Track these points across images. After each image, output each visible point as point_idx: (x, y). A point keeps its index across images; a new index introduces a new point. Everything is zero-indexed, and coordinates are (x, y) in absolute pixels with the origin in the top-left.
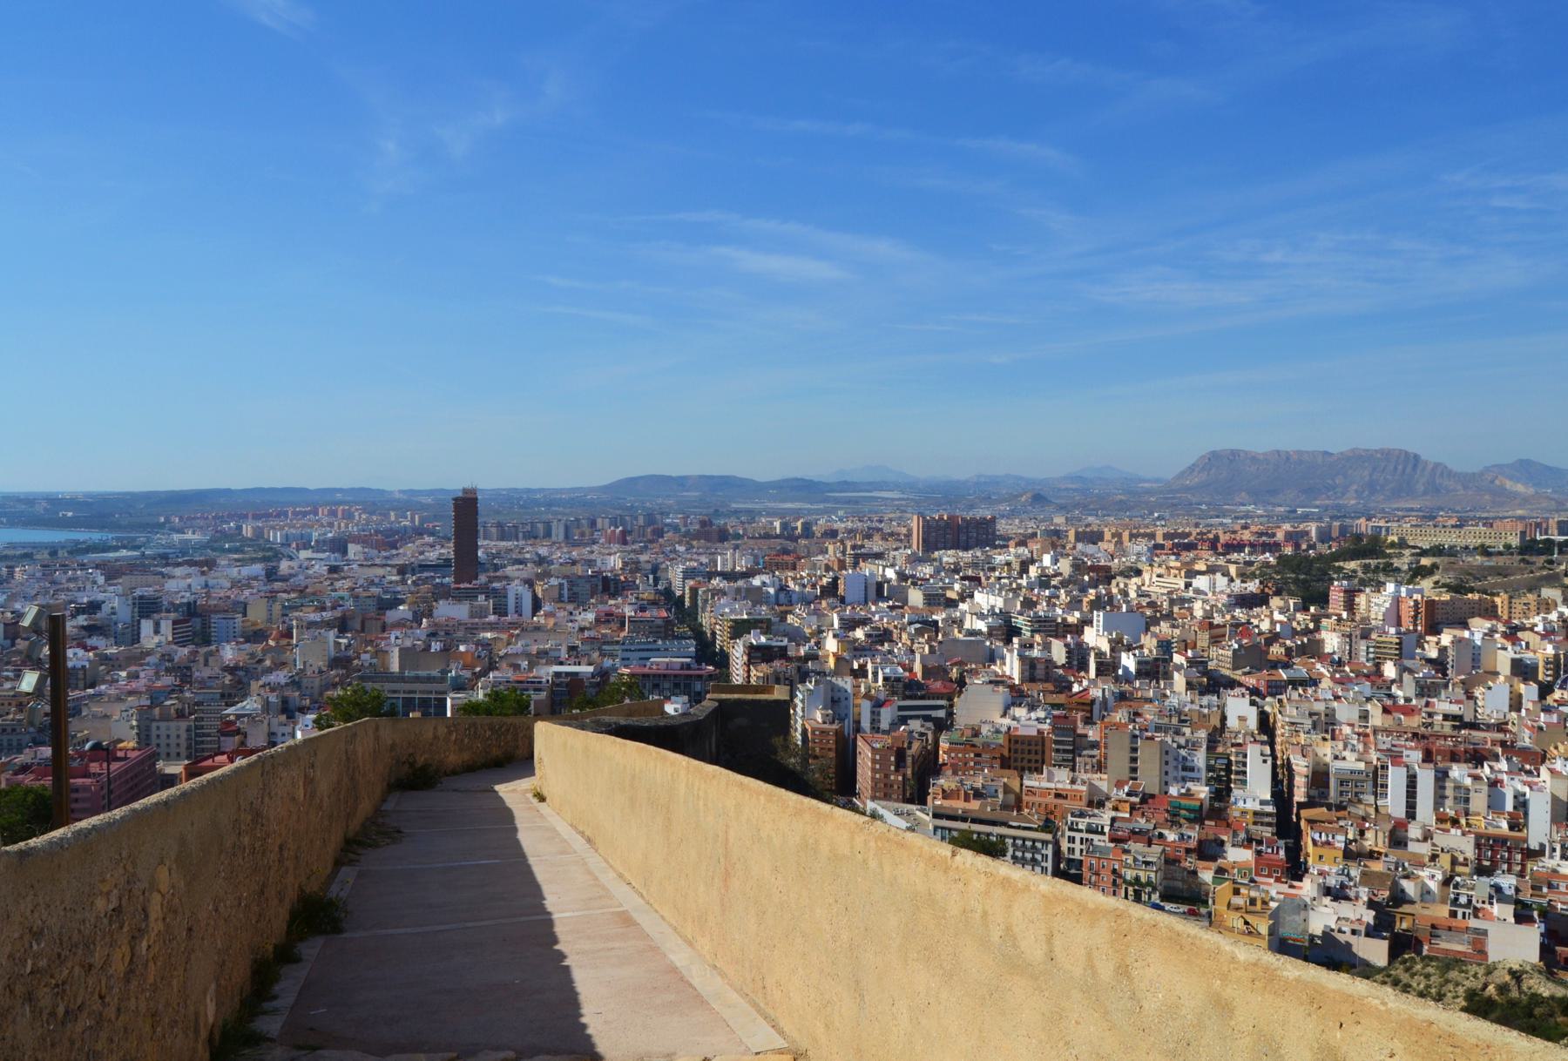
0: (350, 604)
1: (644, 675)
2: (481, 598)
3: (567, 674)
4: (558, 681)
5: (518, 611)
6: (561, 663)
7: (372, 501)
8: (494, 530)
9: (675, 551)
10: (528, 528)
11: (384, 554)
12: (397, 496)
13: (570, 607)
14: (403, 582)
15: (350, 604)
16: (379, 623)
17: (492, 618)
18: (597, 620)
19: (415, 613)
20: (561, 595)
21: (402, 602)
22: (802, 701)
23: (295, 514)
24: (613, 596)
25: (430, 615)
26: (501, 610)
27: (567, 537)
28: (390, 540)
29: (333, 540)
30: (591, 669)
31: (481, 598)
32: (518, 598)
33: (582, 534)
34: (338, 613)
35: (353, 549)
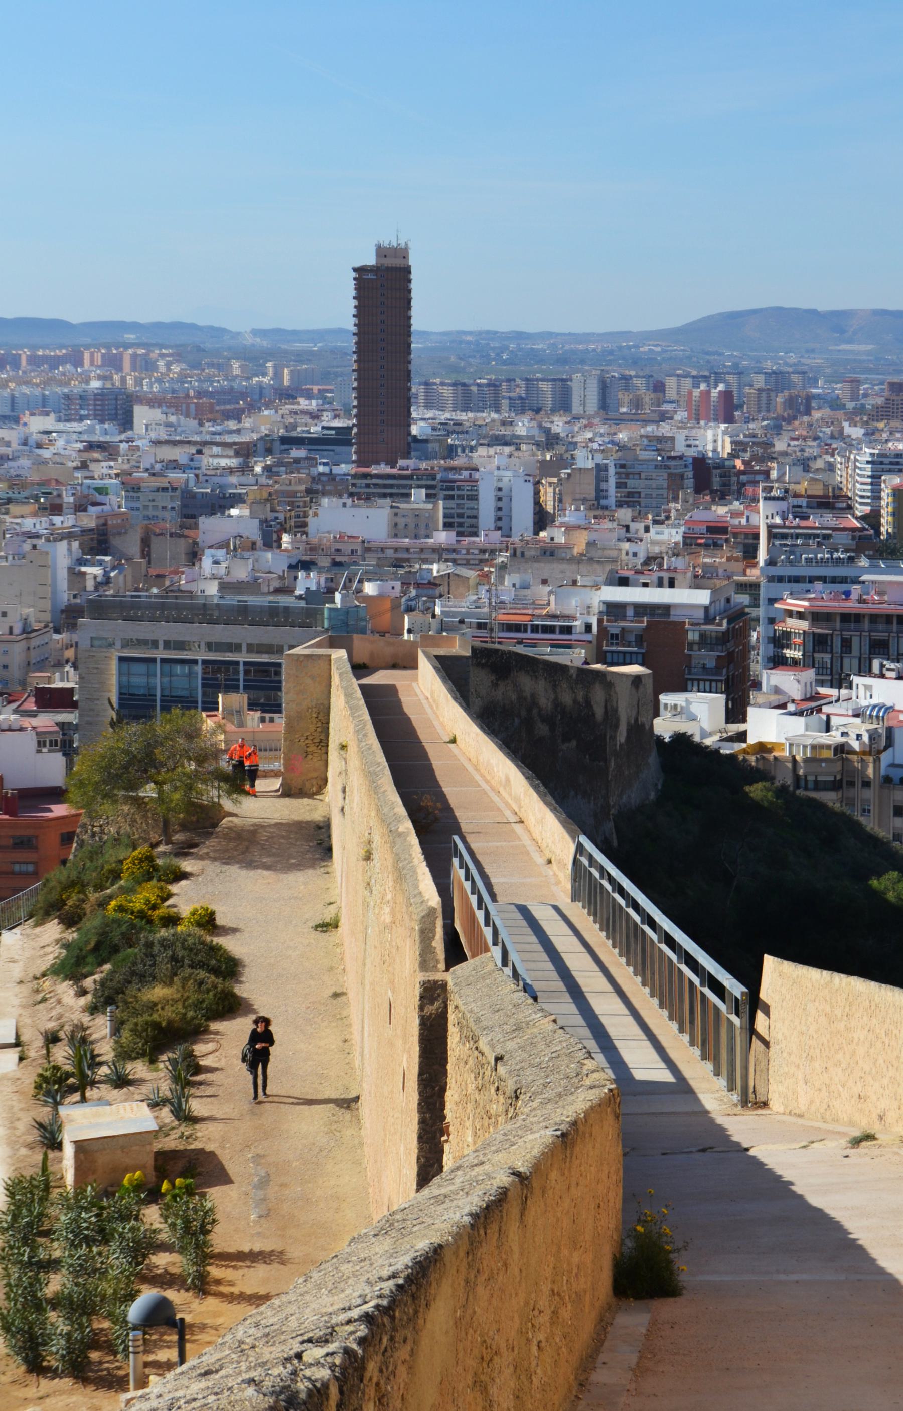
0: (117, 501)
1: (846, 617)
2: (418, 495)
3: (641, 609)
4: (614, 628)
5: (502, 522)
6: (624, 582)
7: (195, 346)
8: (447, 392)
9: (840, 435)
10: (521, 391)
11: (209, 427)
12: (249, 340)
13: (625, 514)
14: (245, 468)
15: (117, 501)
16: (182, 546)
17: (443, 537)
18: (689, 541)
19: (264, 522)
20: (600, 494)
21: (237, 500)
22: (438, 962)
23: (34, 361)
24: (722, 496)
25: (301, 527)
26: (462, 523)
27: (604, 405)
28: (231, 404)
29: (100, 396)
30: (702, 597)
31: (418, 495)
32: (502, 498)
33: (637, 404)
34: (89, 520)
35: (142, 415)
